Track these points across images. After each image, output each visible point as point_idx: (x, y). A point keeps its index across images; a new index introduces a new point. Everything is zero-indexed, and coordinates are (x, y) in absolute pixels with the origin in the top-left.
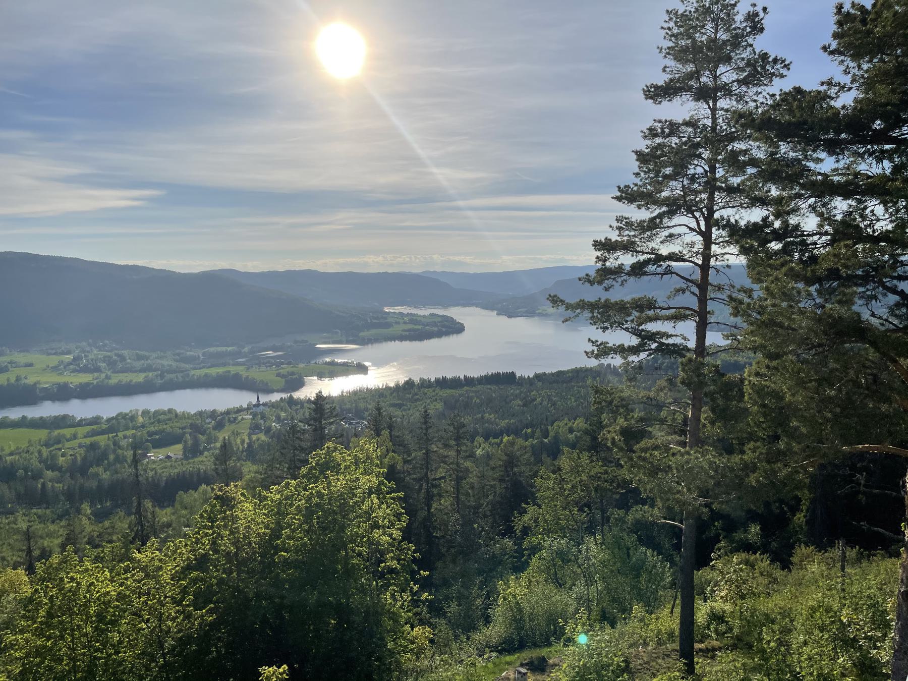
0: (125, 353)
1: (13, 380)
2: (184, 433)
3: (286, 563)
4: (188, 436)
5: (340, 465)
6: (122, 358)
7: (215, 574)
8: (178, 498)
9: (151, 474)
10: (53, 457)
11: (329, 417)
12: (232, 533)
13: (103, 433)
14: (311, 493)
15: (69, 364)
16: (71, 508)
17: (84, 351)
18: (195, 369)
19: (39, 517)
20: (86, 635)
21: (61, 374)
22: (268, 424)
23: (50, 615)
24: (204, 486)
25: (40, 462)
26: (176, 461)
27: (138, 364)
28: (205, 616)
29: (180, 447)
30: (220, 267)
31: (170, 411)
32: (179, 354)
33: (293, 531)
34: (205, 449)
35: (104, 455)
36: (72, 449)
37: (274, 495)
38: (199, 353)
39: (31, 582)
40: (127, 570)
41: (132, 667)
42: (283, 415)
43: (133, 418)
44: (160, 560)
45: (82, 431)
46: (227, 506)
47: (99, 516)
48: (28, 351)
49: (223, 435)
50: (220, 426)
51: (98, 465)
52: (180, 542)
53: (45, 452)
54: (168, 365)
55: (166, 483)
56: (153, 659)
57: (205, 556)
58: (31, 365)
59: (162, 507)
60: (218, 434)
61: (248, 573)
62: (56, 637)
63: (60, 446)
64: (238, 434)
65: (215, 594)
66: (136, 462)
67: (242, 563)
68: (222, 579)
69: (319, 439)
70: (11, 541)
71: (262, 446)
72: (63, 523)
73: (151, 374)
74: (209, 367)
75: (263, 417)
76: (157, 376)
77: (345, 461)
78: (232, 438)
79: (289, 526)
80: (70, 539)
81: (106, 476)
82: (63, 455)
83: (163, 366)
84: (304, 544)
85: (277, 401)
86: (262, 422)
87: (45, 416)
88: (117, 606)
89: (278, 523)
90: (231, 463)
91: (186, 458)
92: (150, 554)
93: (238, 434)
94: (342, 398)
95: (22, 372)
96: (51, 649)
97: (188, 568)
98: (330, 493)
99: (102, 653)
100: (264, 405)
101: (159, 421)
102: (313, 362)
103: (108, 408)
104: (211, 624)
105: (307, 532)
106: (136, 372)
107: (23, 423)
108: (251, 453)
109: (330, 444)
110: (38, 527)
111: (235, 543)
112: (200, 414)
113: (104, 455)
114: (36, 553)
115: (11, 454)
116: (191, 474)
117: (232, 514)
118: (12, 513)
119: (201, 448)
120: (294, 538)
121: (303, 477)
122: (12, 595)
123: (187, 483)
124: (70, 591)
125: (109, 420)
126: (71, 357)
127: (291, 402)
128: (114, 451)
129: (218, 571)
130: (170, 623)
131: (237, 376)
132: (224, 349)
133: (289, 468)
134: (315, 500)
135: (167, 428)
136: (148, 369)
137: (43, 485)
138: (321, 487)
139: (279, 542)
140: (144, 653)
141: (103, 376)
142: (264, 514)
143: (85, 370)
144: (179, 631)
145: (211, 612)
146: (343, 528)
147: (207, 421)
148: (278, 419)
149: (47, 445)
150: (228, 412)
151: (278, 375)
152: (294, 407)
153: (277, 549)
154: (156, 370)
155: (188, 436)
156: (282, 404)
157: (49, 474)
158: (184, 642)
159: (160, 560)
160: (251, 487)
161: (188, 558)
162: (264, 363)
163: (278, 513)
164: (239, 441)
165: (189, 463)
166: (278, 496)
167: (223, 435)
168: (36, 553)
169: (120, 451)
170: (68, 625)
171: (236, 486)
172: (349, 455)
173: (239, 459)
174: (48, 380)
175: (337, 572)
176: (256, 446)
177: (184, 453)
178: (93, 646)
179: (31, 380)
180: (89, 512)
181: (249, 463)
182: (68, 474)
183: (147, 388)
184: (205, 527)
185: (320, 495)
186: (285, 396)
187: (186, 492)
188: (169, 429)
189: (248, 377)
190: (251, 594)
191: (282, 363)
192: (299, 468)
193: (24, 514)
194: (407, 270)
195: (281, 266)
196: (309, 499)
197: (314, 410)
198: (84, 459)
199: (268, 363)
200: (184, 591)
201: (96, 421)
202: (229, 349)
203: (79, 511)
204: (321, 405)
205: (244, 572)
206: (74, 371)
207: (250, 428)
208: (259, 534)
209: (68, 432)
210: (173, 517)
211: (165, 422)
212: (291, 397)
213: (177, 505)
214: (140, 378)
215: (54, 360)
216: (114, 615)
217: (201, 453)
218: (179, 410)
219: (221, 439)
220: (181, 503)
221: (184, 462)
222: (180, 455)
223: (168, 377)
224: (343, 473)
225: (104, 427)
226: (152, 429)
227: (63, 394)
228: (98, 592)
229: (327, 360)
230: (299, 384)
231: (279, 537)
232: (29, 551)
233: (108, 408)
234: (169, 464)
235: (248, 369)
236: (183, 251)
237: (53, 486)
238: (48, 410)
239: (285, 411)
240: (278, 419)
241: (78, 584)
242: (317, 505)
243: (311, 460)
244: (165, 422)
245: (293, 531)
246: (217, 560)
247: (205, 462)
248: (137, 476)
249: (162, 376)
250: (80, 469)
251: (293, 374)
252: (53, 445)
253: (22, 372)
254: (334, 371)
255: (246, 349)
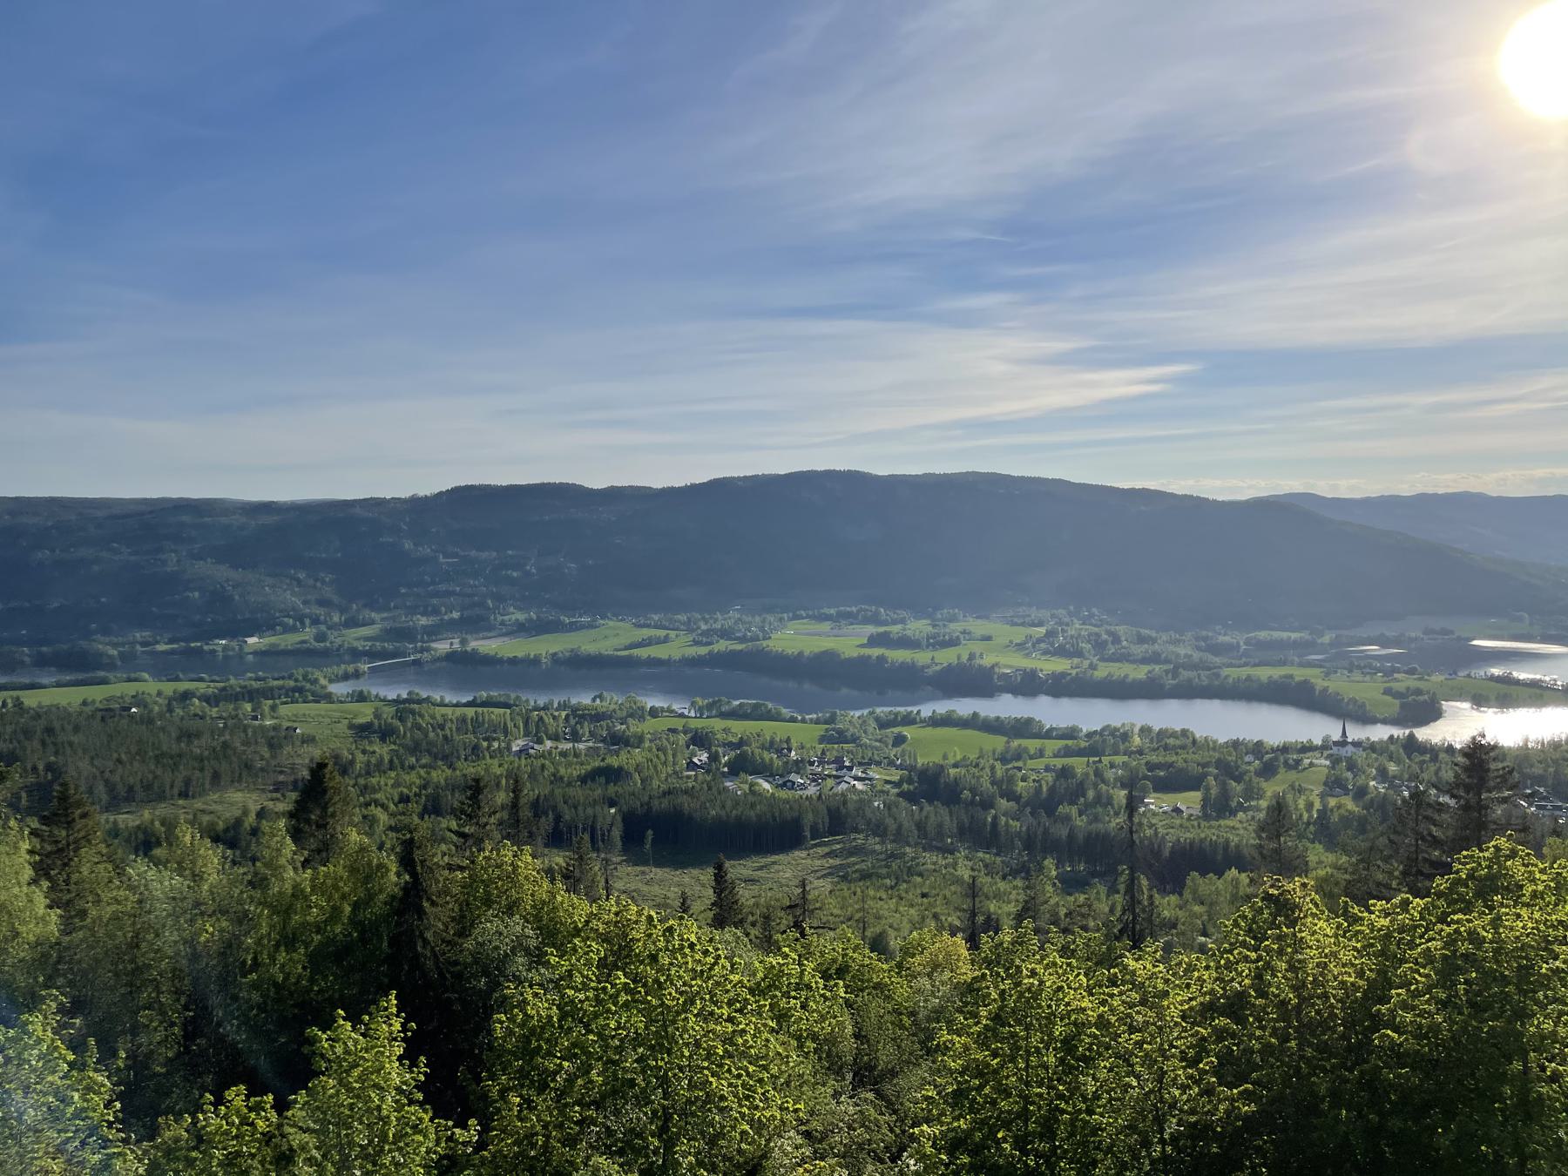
0: (1121, 630)
1: (965, 658)
2: (1205, 775)
3: (1397, 1056)
4: (1210, 778)
5: (1522, 887)
6: (1116, 639)
7: (1258, 1037)
8: (1189, 882)
9: (1149, 832)
10: (1011, 780)
11: (1498, 788)
12: (1292, 968)
13: (1080, 753)
14: (1457, 931)
15: (1039, 641)
16: (1030, 861)
17: (1060, 623)
18: (1230, 665)
19: (986, 866)
20: (1046, 1067)
21: (1028, 655)
22: (1361, 781)
23: (997, 1018)
24: (1234, 871)
25: (993, 783)
26: (1189, 819)
27: (1139, 650)
28: (1233, 1102)
29: (1195, 796)
30: (1287, 491)
31: (1184, 732)
32: (1205, 639)
33: (1416, 994)
34: (1240, 807)
35: (1080, 790)
36: (1034, 775)
37: (1377, 917)
38: (832, 611)
39: (973, 962)
40: (1113, 982)
41: (1113, 1145)
42: (1392, 768)
43: (1125, 737)
44: (1167, 981)
45: (1053, 745)
46: (1287, 917)
47: (1070, 884)
48: (987, 617)
49: (1272, 788)
50: (1268, 771)
51: (1072, 803)
52: (1198, 959)
53: (1000, 770)
54: (1186, 656)
55: (1172, 852)
56: (1146, 1144)
57: (1241, 995)
58: (989, 638)
59: (1164, 892)
60: (1264, 785)
61: (1317, 1049)
62: (1004, 1055)
63: (1020, 764)
64: (1301, 791)
65: (1257, 1068)
66: (1131, 806)
67: (1306, 1029)
68: (1270, 1045)
69: (1475, 828)
70: (948, 894)
71: (1346, 820)
72: (1019, 883)
73: (1157, 668)
74: (1255, 665)
75: (1352, 766)
76: (1167, 672)
77: (1533, 881)
78: (1289, 797)
79: (1406, 984)
80: (1027, 910)
81: (1080, 822)
82: (1024, 780)
83: (1178, 655)
84: (1435, 1029)
85: (1381, 741)
86: (1349, 775)
87: (1003, 716)
88: (1095, 1036)
89: (1382, 972)
90: (1287, 841)
91: (1206, 817)
92: (1149, 966)
93: (1301, 791)
94: (1524, 755)
95: (976, 647)
96: (996, 1072)
97: (1209, 1010)
98: (1497, 940)
99: (1067, 1103)
100: (1356, 744)
101: (1166, 748)
102: (1461, 674)
103: (1091, 716)
104: (1247, 1118)
105: (1444, 1004)
106: (1133, 662)
107: (973, 723)
108: (1325, 831)
109: (1502, 842)
110: (983, 880)
111: (1298, 988)
112: (1236, 744)
113: (1080, 790)
114: (980, 919)
115: (956, 766)
116: (1213, 845)
117: (1294, 935)
118: (952, 853)
119: (1234, 804)
120: (1413, 1010)
121: (1439, 895)
122: (947, 974)
123: (1209, 859)
124: (1029, 990)
125: (1090, 735)
126: (1042, 630)
127: (1411, 745)
128: (1095, 785)
129: (1263, 1028)
130: (1177, 1093)
131: (1306, 686)
132: (1285, 635)
133: (1405, 873)
134: (1464, 947)
135: (1178, 760)
136: (1154, 659)
137: (995, 818)
138: (1479, 922)
139: (1384, 1009)
140: (1132, 1128)
141: (1086, 663)
142: (1355, 949)
143: (1061, 652)
144: (1193, 1112)
145: (1247, 1096)
146: (1523, 1015)
147: (1248, 758)
148: (1383, 774)
149: (1004, 760)
150: (1285, 749)
151: (1388, 692)
152: (1418, 758)
153: (1377, 1023)
154: (1167, 661)
155: (1210, 778)
156: (1392, 748)
157: (1003, 803)
158: (1199, 1131)
159: (1167, 981)
160: (1326, 889)
161: (1212, 993)
162: (1359, 667)
163: (1382, 953)
164: (1301, 803)
165: (1210, 827)
166: (1385, 922)
167: (1272, 788)
168: (980, 919)
169: (1103, 787)
170: (1023, 1043)
171: (1304, 885)
172: (1542, 871)
173: (1300, 837)
174: (1011, 663)
175: (1502, 1100)
176: (1335, 818)
177: (1204, 807)
178: (1054, 1088)
179: (988, 661)
180: (1054, 873)
181: (1319, 847)
182: (1028, 810)
183: (1150, 691)
184: (1244, 944)
185: (1473, 937)
186: (1399, 732)
187: (1203, 874)
188: (1180, 764)
189: (1325, 689)
190: (1323, 1090)
191: (1394, 670)
192: (1431, 877)
193: (967, 857)
194: (1430, 491)
195: (1408, 485)
196: (1451, 942)
197: (1466, 769)
198: (1052, 790)
199: (1367, 667)
200: (1201, 1046)
201: (1071, 733)
202: (1294, 636)
203: (1041, 869)
204: (1482, 761)
205: (1310, 1045)
206: (1045, 653)
207: (1325, 784)
208: (1343, 982)
209: (1032, 745)
210: (1180, 913)
211: (1174, 749)
212: (1411, 736)
213: (1187, 894)
214: (1139, 673)
215: (1019, 634)
216: (1090, 1049)
217: (1233, 813)
218: (1199, 734)
219: (1269, 794)
220: (1195, 892)
221: (1203, 824)
222: (1197, 810)
223: (1185, 674)
224: (1527, 905)
225: (1083, 744)
226: (1154, 758)
227: (1028, 685)
228: (1068, 1004)
229: (1496, 671)
230: (1431, 714)
231: (1384, 1000)
232: (974, 914)
233: (1091, 716)
234: (1178, 822)
235: (1327, 674)
236: (1230, 464)
237: (1007, 824)
238: (1007, 707)
239: (1398, 762)
240: (1383, 774)
241: (1042, 982)
242: (1465, 956)
243: (1456, 866)
244: (1174, 749)
245: (1416, 994)
246: (1264, 1009)
247: (1240, 830)
248: (1131, 832)
249: (1175, 673)
250: (1045, 804)
251: (1419, 692)
252: (1010, 761)
253: (976, 647)
254: (1508, 694)
255: (1326, 639)
